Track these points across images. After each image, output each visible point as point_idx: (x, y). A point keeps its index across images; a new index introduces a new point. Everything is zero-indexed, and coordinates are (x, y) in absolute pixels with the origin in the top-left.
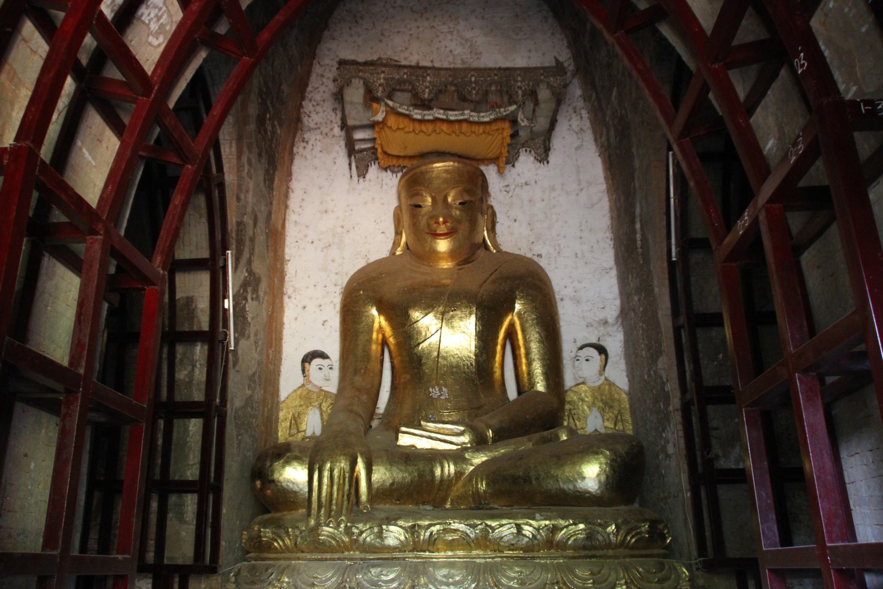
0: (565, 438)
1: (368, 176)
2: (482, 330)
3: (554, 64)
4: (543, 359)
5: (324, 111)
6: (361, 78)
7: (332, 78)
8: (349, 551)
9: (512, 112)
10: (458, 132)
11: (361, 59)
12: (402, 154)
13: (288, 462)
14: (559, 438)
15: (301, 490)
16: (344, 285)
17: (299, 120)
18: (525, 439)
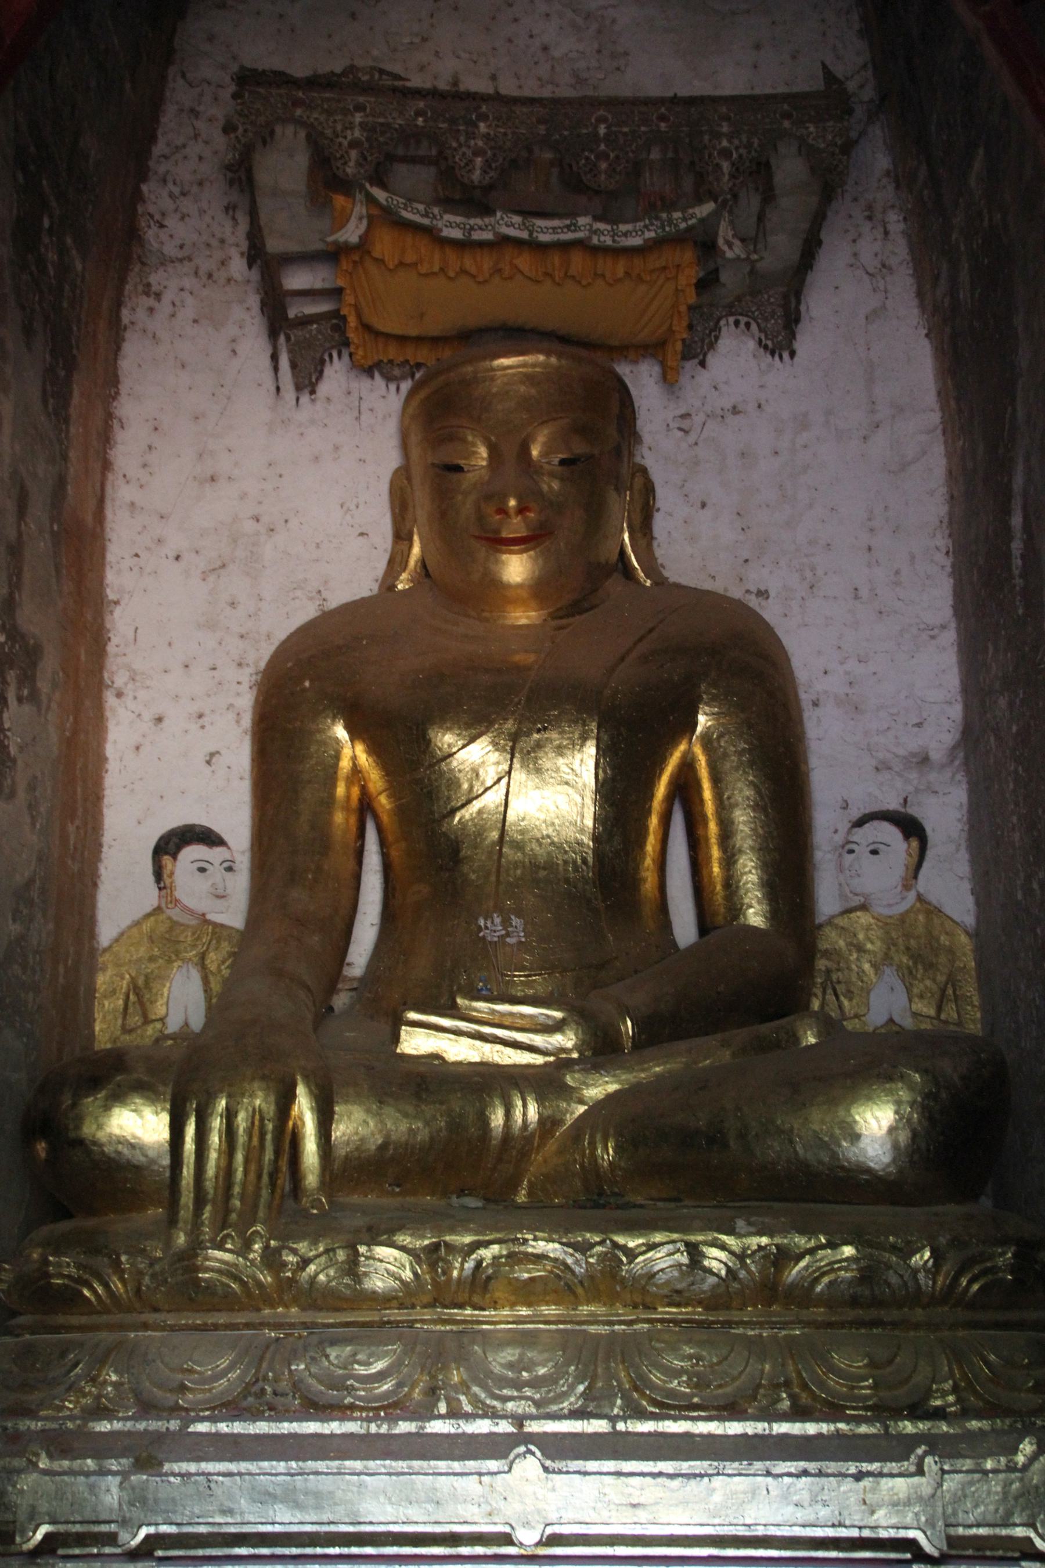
0: (812, 1040)
1: (324, 388)
2: (613, 779)
3: (819, 85)
4: (762, 850)
5: (202, 212)
6: (299, 122)
7: (221, 123)
8: (273, 1306)
9: (702, 221)
10: (558, 275)
11: (299, 70)
12: (413, 332)
13: (118, 1097)
14: (797, 1040)
15: (153, 1161)
16: (262, 665)
17: (133, 235)
18: (712, 1041)
